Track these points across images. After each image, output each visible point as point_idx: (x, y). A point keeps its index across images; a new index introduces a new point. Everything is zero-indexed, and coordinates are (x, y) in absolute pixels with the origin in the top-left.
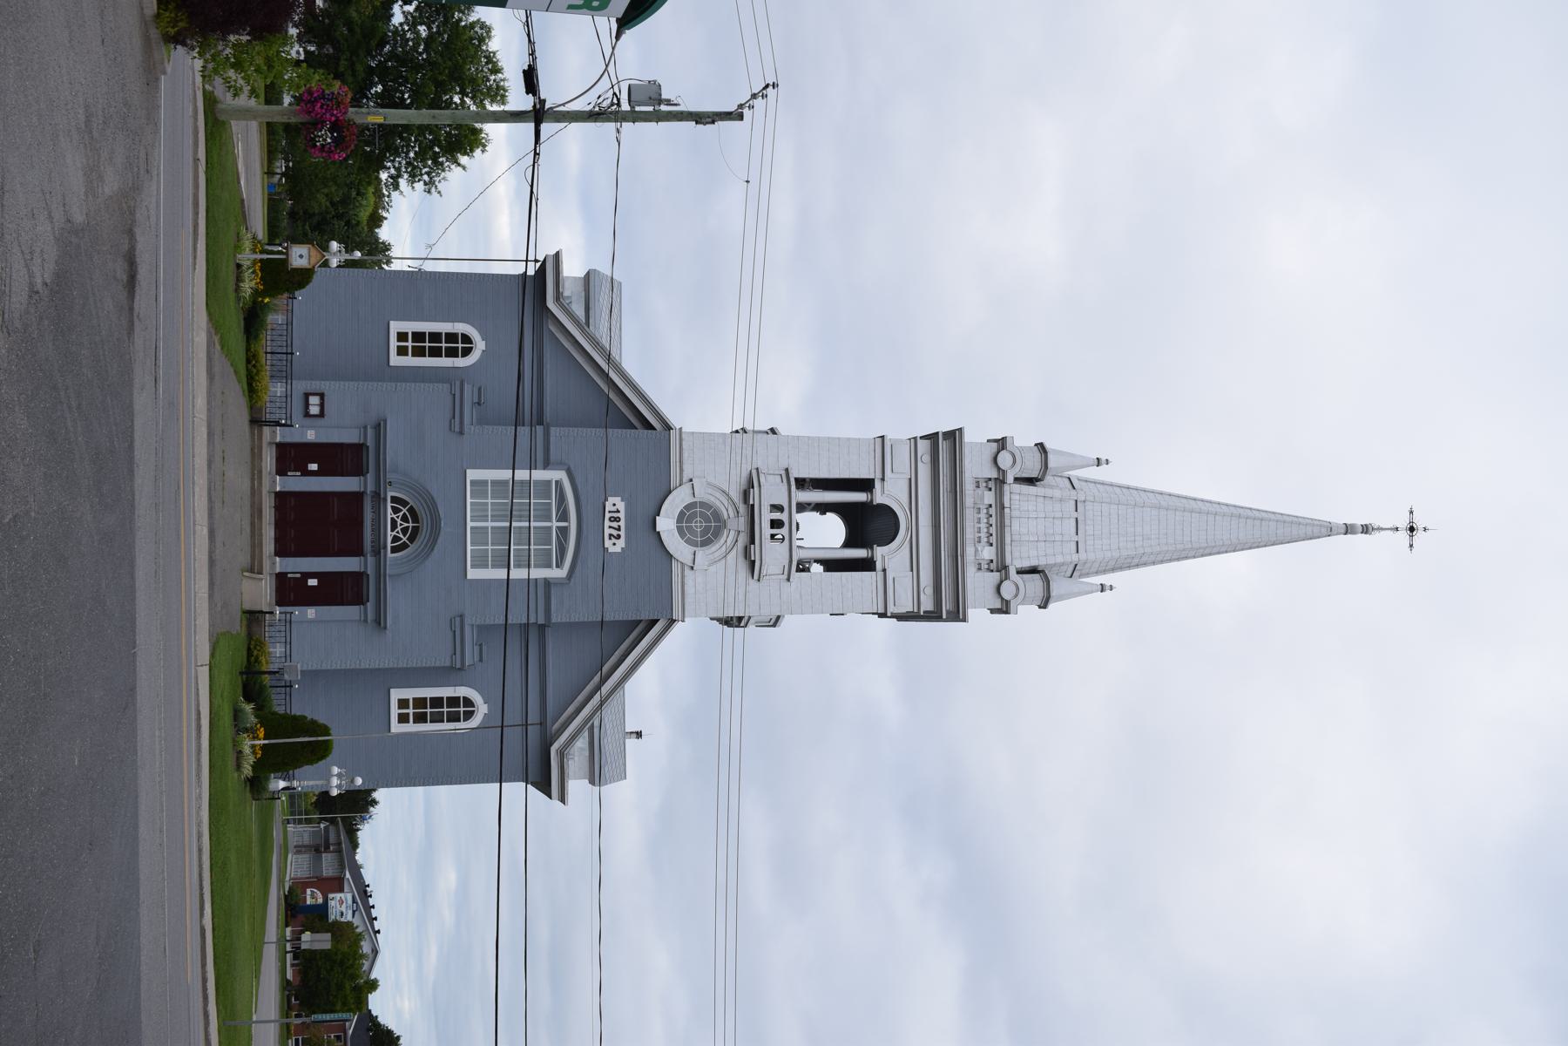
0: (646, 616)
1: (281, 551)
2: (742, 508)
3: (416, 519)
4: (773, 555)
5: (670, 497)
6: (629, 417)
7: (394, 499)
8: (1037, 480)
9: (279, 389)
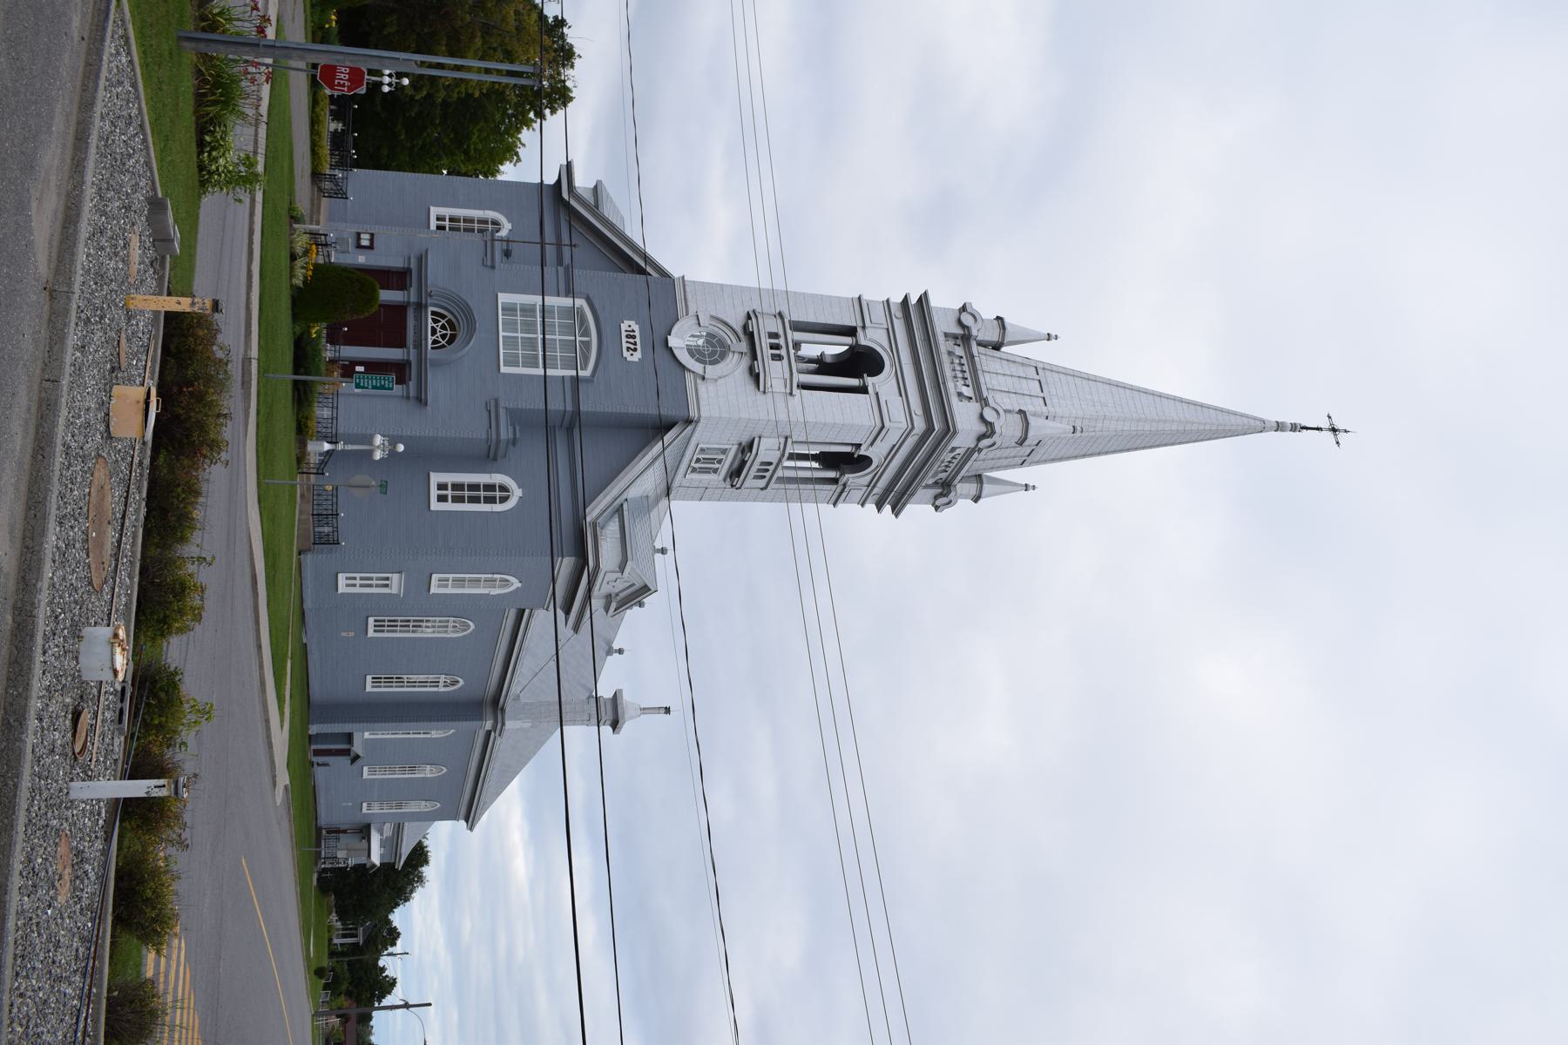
4: (776, 373)
7: (433, 313)
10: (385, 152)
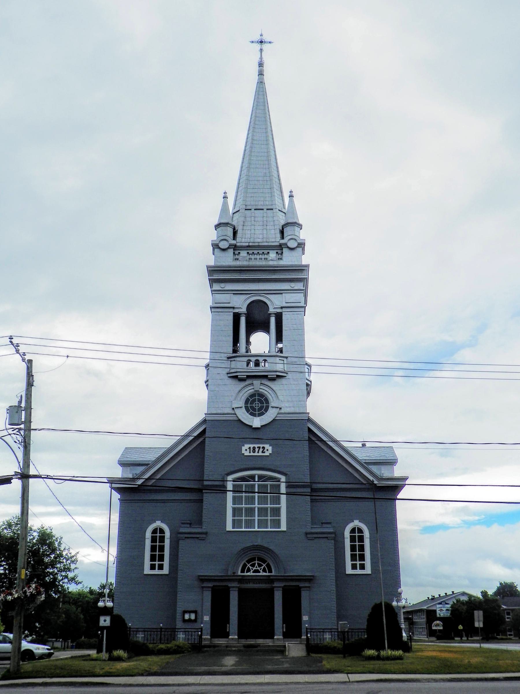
0: (306, 435)
1: (271, 635)
2: (248, 382)
3: (253, 559)
5: (242, 420)
6: (198, 443)
7: (243, 571)
8: (234, 229)
9: (181, 636)
10: (80, 603)
